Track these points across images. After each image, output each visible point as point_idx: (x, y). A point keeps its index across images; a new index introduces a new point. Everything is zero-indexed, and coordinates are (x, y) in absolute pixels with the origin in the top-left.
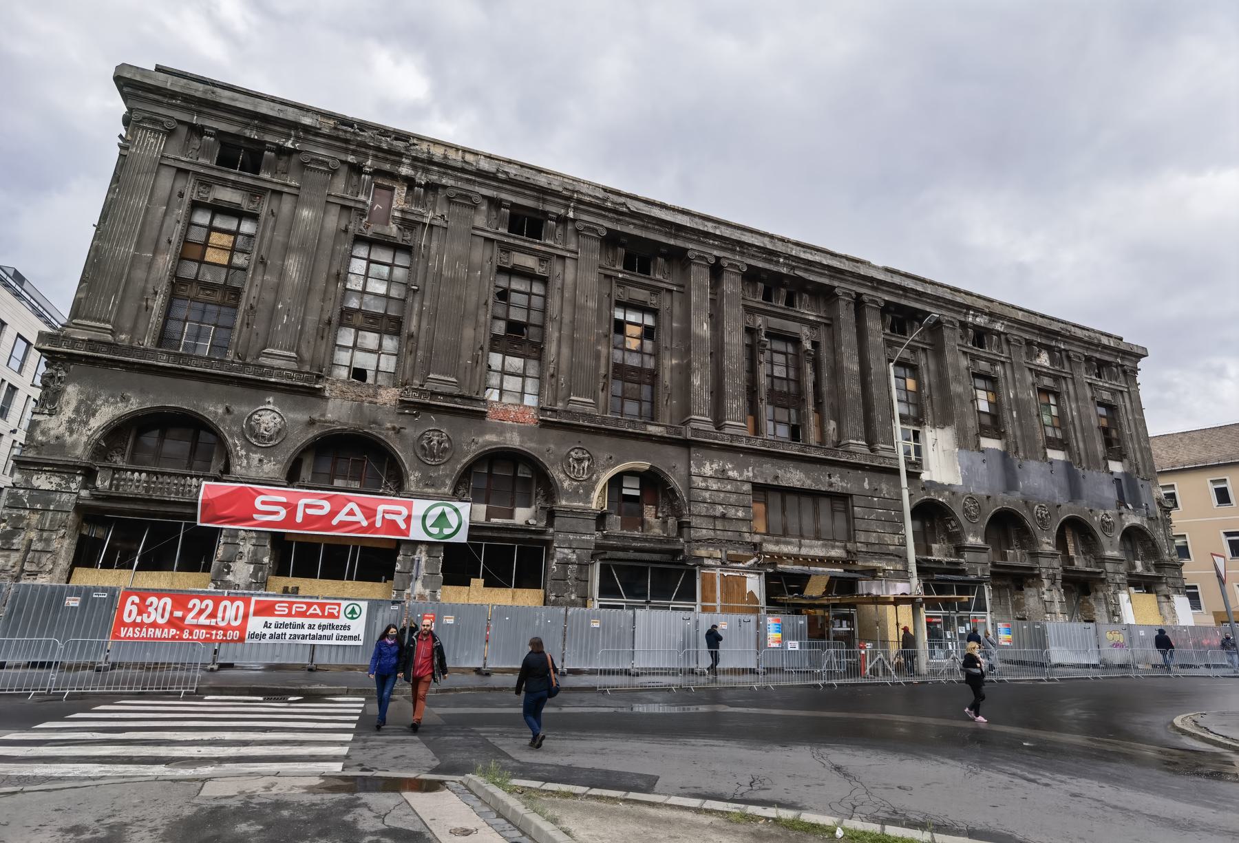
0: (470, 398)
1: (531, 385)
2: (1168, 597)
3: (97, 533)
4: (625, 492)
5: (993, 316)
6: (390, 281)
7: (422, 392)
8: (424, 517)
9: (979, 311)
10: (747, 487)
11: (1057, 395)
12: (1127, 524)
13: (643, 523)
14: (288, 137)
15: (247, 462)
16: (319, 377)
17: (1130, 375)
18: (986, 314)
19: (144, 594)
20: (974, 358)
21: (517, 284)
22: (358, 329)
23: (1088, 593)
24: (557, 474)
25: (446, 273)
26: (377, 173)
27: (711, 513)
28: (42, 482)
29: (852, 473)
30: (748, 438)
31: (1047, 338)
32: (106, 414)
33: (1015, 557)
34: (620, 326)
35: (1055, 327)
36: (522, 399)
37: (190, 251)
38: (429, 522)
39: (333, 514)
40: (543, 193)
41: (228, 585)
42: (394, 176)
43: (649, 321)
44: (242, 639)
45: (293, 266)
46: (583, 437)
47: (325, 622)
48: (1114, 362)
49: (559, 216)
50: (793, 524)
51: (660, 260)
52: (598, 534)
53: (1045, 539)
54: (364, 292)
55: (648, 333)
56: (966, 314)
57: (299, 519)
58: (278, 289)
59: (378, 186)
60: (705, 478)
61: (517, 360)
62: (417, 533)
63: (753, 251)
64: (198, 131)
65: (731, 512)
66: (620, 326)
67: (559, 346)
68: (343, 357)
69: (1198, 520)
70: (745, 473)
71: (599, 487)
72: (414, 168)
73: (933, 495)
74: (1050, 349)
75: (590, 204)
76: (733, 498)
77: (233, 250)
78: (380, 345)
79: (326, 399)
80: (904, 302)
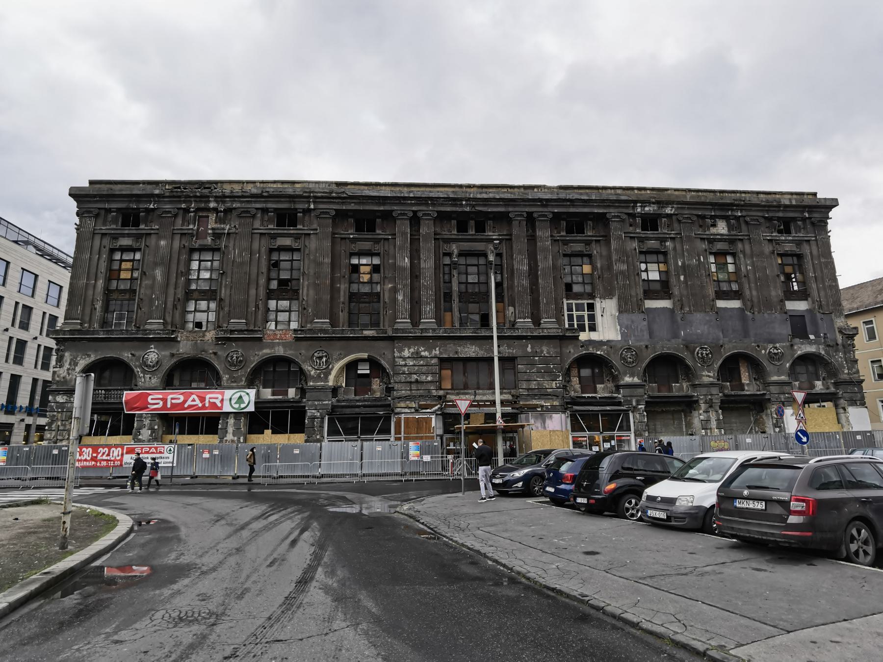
1: (294, 316)
2: (844, 409)
3: (103, 418)
4: (359, 372)
5: (660, 203)
6: (211, 270)
8: (230, 399)
9: (645, 203)
11: (734, 255)
15: (144, 379)
16: (173, 331)
18: (654, 203)
19: (110, 447)
20: (642, 240)
21: (284, 256)
24: (306, 367)
29: (517, 342)
30: (434, 330)
31: (722, 210)
34: (355, 269)
36: (289, 325)
37: (112, 274)
38: (233, 402)
39: (185, 401)
40: (292, 198)
41: (140, 441)
43: (376, 261)
44: (121, 465)
45: (158, 273)
46: (323, 343)
49: (304, 209)
55: (376, 269)
56: (634, 207)
57: (169, 406)
58: (152, 287)
60: (404, 359)
61: (285, 302)
62: (227, 408)
63: (441, 201)
65: (423, 378)
66: (355, 269)
67: (308, 290)
68: (190, 317)
70: (434, 352)
74: (726, 218)
75: (322, 197)
76: (424, 369)
77: (132, 270)
78: (208, 307)
80: (572, 210)
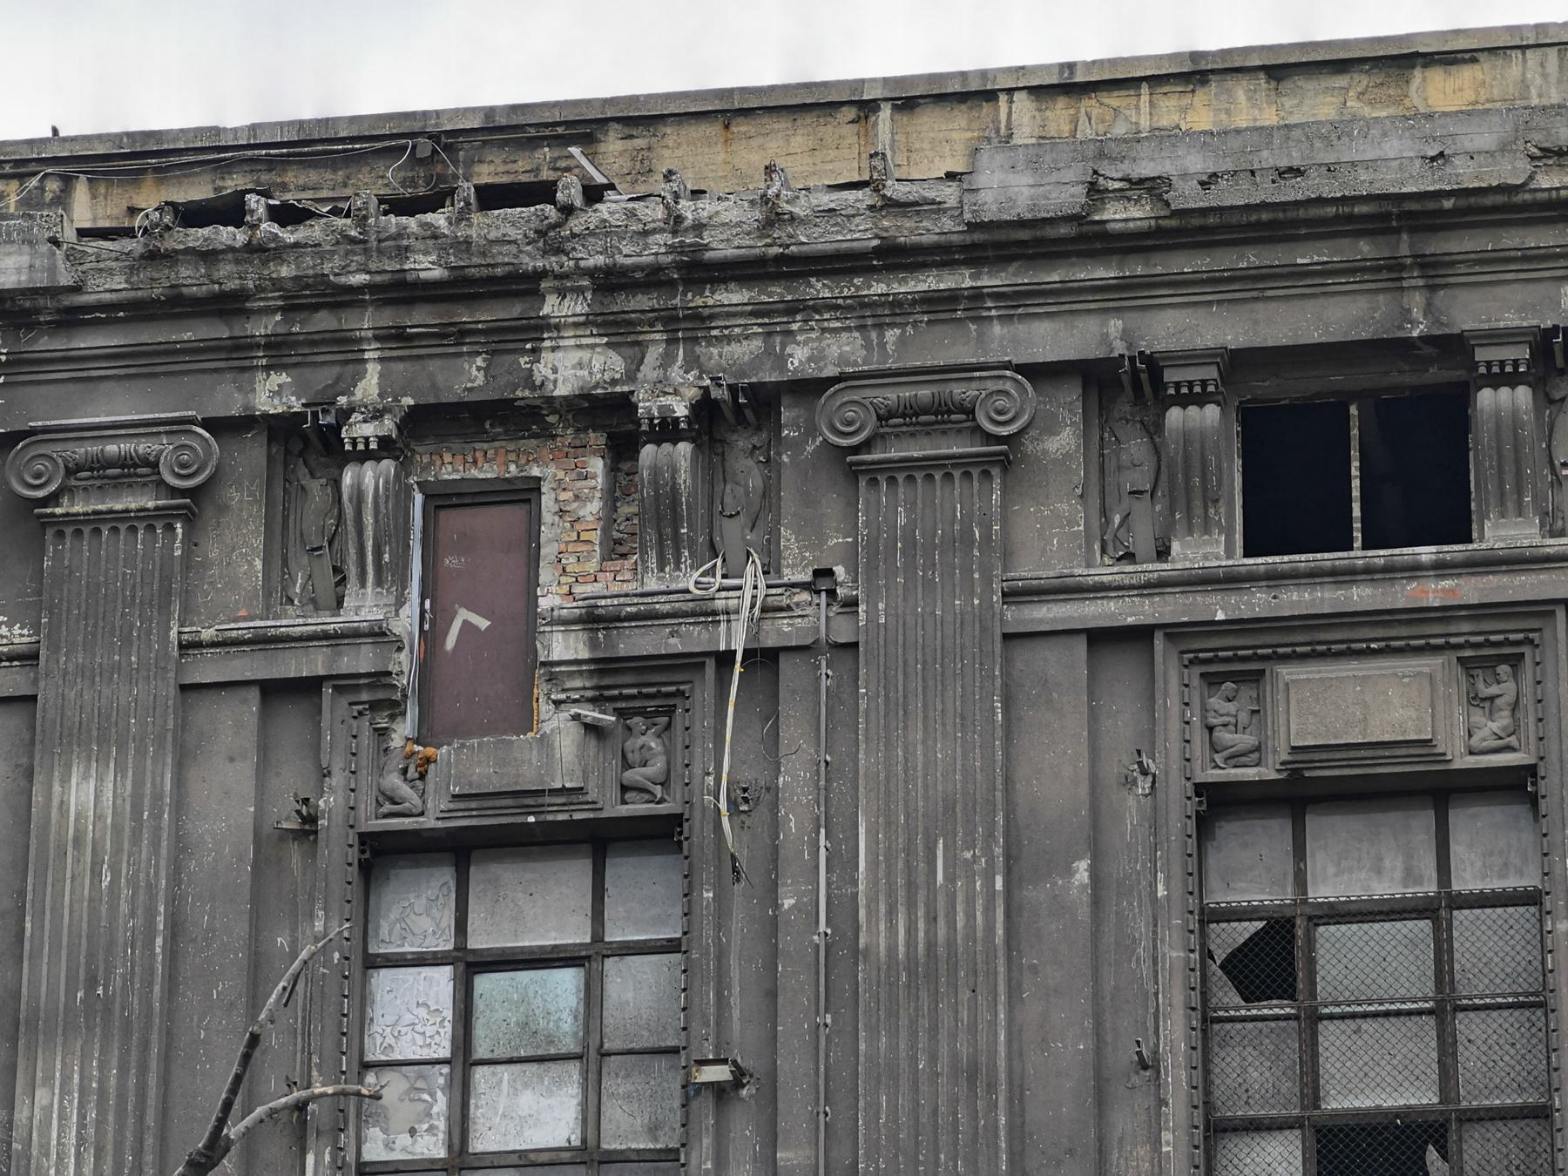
6: (592, 1057)
21: (1357, 862)
26: (429, 423)
40: (1410, 228)
42: (519, 417)
59: (442, 499)
72: (617, 330)
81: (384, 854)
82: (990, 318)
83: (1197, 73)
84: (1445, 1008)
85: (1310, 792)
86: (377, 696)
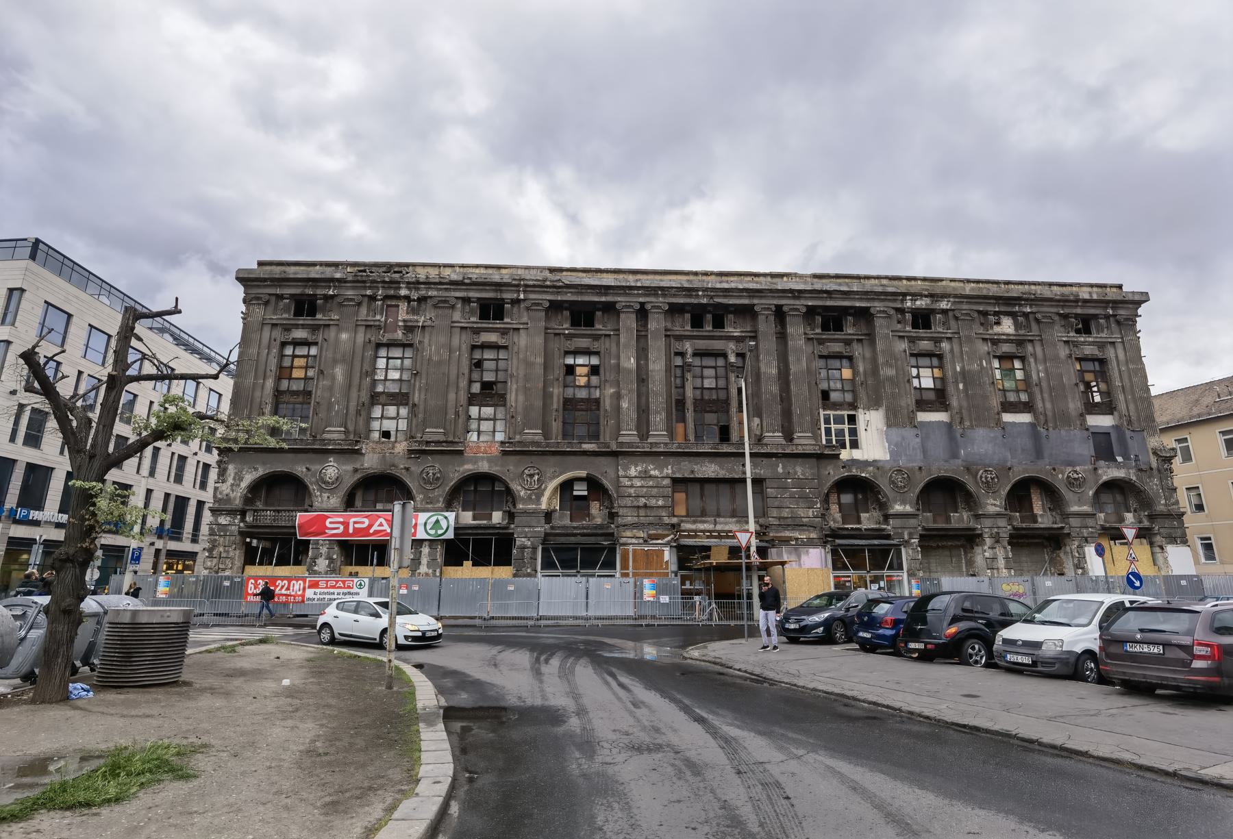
0: (452, 442)
1: (500, 425)
4: (575, 493)
6: (402, 369)
7: (420, 443)
9: (916, 296)
10: (667, 482)
11: (1023, 359)
12: (1105, 478)
13: (589, 515)
14: (329, 288)
15: (322, 499)
17: (1128, 324)
20: (912, 340)
21: (489, 354)
22: (383, 405)
23: (1060, 548)
24: (515, 486)
25: (435, 358)
26: (386, 297)
27: (635, 504)
28: (223, 520)
30: (666, 444)
32: (249, 478)
33: (961, 519)
34: (570, 370)
35: (1015, 291)
37: (283, 372)
38: (428, 527)
39: (370, 526)
40: (499, 286)
42: (398, 298)
43: (595, 361)
45: (339, 372)
46: (534, 458)
47: (346, 591)
48: (1103, 318)
50: (711, 506)
51: (599, 314)
52: (547, 526)
53: (991, 501)
54: (386, 379)
55: (595, 370)
56: (902, 301)
57: (351, 531)
58: (331, 388)
59: (388, 306)
63: (673, 291)
64: (280, 297)
65: (653, 502)
66: (570, 370)
67: (517, 395)
68: (376, 425)
69: (1204, 466)
71: (547, 494)
72: (409, 289)
73: (854, 472)
74: (1013, 315)
75: (534, 286)
77: (306, 368)
79: (363, 455)
80: (829, 303)
81: (379, 346)
82: (1013, 745)
83: (477, 266)
84: (497, 370)
85: (485, 346)
86: (379, 328)
